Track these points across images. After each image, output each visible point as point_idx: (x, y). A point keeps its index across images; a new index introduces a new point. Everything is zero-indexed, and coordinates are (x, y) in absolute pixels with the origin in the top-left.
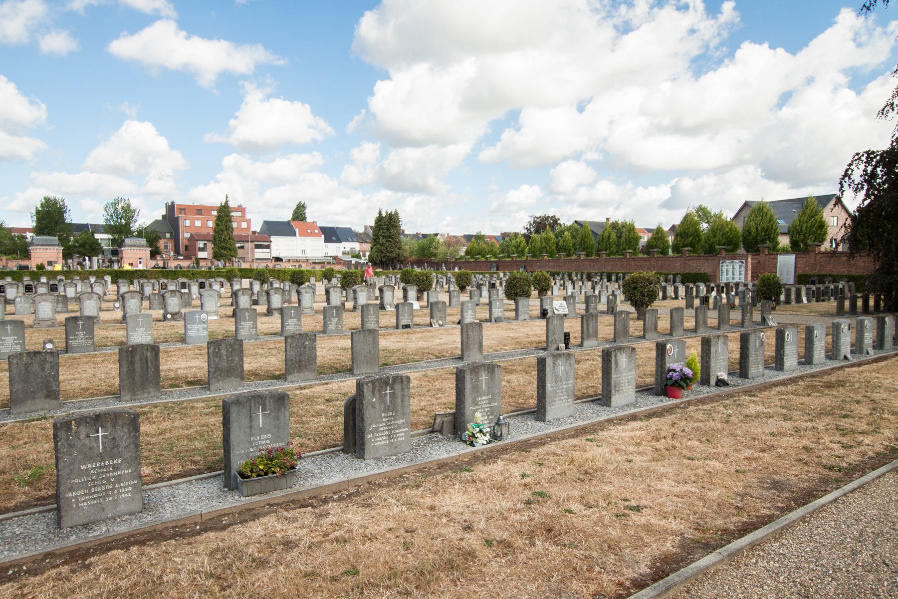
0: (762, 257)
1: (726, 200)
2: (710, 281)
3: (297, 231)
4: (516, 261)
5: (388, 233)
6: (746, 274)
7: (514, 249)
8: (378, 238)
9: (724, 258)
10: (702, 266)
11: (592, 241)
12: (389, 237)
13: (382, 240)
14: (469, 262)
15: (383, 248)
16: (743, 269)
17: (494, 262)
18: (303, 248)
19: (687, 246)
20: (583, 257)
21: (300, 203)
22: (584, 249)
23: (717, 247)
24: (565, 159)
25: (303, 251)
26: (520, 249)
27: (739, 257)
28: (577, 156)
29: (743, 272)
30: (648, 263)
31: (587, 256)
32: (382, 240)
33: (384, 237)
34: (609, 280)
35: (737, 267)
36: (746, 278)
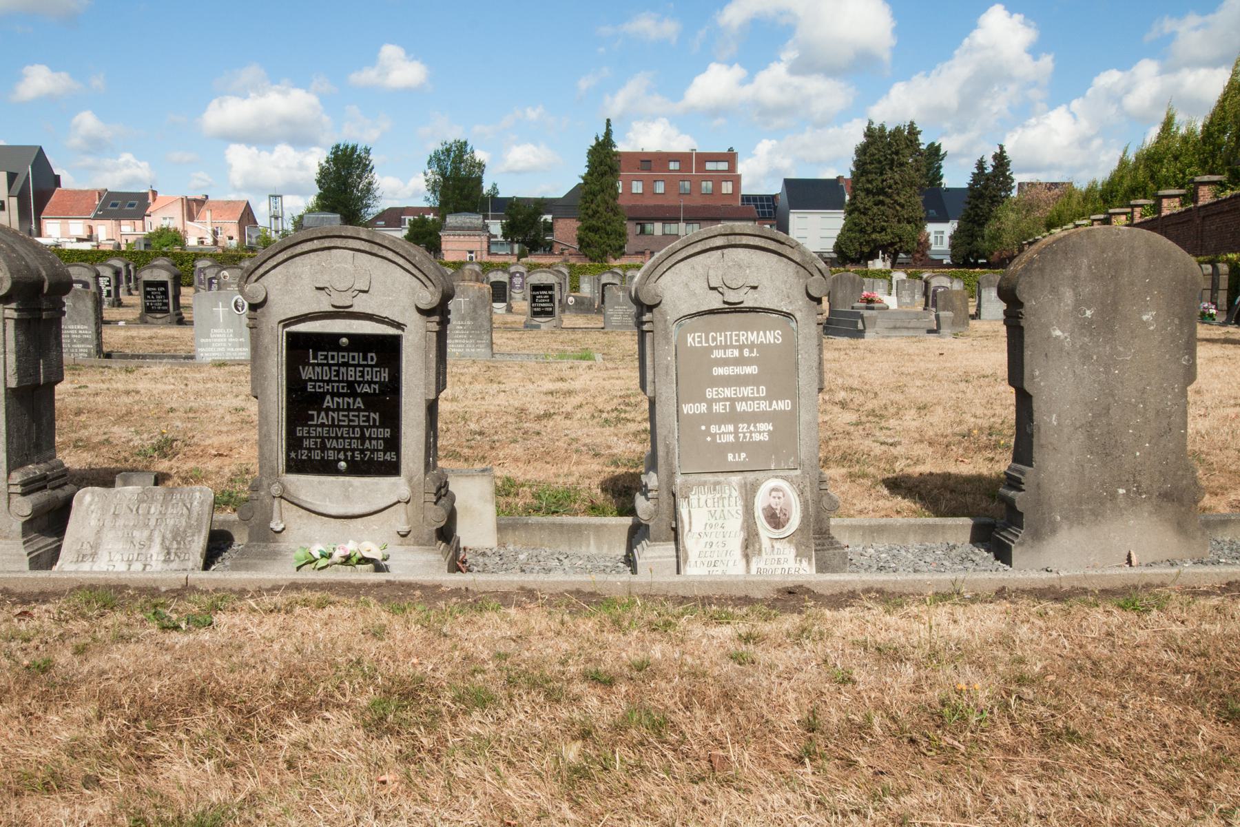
12: (881, 191)
15: (864, 220)
33: (868, 192)
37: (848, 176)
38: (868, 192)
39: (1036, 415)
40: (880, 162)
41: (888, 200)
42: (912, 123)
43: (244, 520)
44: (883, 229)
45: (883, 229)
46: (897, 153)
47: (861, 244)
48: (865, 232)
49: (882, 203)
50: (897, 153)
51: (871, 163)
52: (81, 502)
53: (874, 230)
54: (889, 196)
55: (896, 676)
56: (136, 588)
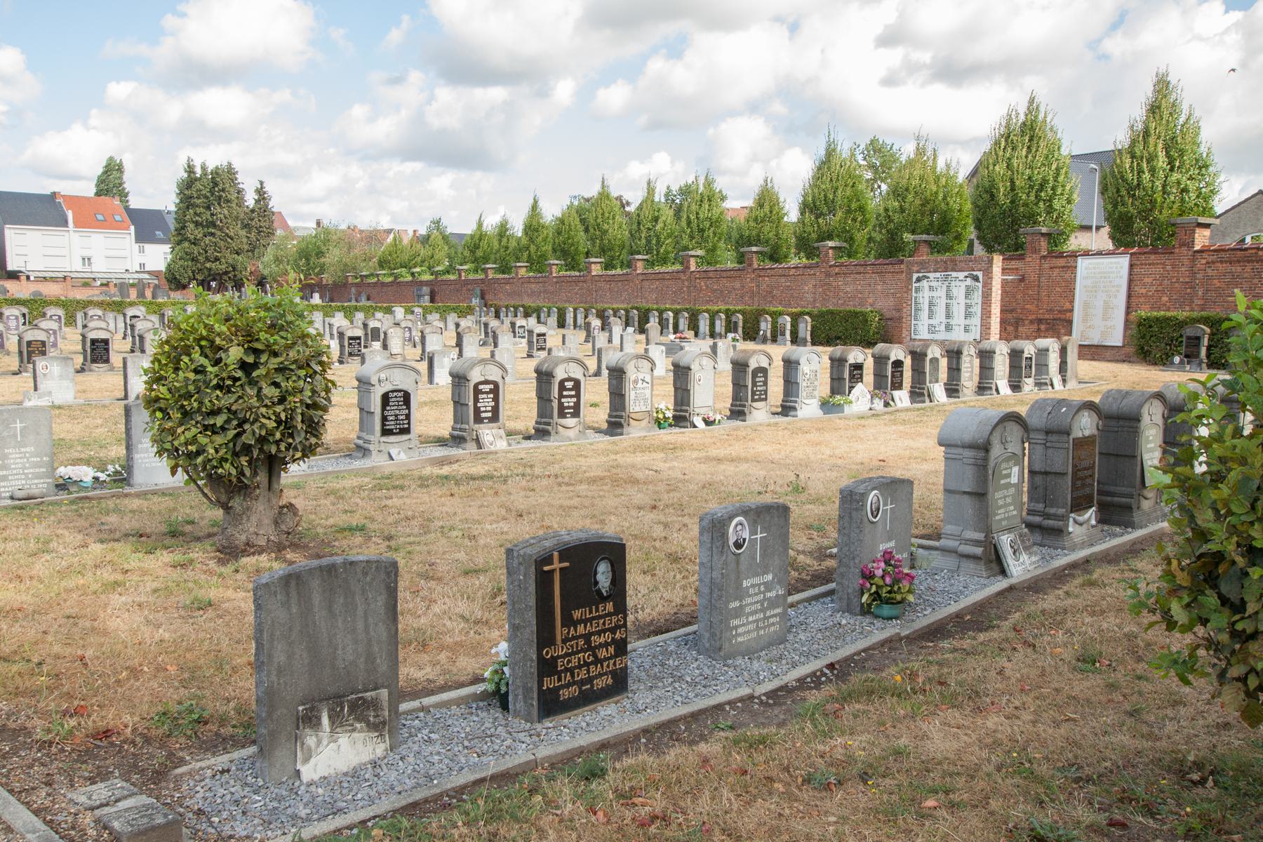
0: (1030, 265)
1: (954, 130)
2: (888, 337)
3: (70, 215)
4: (467, 282)
5: (207, 216)
6: (986, 314)
7: (467, 253)
8: (183, 228)
9: (923, 266)
10: (865, 292)
11: (618, 231)
12: (213, 225)
13: (192, 231)
14: (383, 284)
15: (196, 250)
16: (977, 297)
17: (427, 283)
18: (86, 253)
19: (830, 237)
20: (596, 270)
21: (111, 159)
22: (603, 251)
23: (908, 237)
24: (732, 113)
25: (87, 260)
26: (479, 253)
27: (967, 263)
28: (754, 108)
29: (977, 309)
30: (737, 285)
31: (608, 266)
32: (192, 231)
33: (197, 224)
34: (694, 326)
35: (959, 291)
36: (985, 327)
37: (173, 208)
38: (197, 224)
39: (1124, 387)
40: (206, 197)
41: (219, 233)
42: (230, 164)
43: (1212, 334)
44: (217, 259)
45: (217, 259)
46: (223, 190)
47: (193, 272)
48: (197, 261)
49: (213, 234)
50: (223, 190)
51: (198, 198)
52: (336, 215)
53: (208, 259)
54: (221, 230)
55: (1196, 756)
56: (972, 613)
